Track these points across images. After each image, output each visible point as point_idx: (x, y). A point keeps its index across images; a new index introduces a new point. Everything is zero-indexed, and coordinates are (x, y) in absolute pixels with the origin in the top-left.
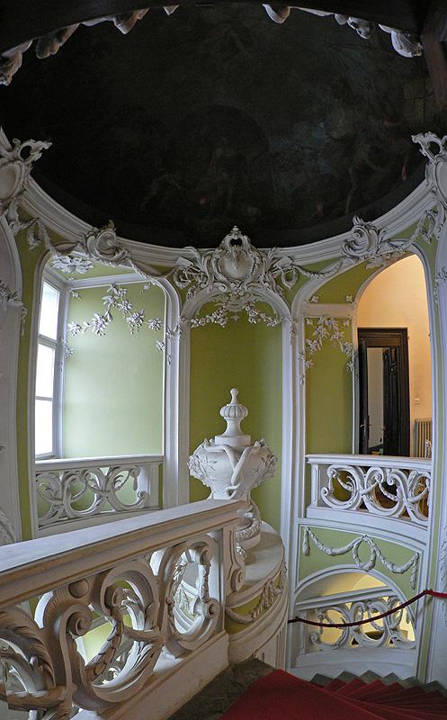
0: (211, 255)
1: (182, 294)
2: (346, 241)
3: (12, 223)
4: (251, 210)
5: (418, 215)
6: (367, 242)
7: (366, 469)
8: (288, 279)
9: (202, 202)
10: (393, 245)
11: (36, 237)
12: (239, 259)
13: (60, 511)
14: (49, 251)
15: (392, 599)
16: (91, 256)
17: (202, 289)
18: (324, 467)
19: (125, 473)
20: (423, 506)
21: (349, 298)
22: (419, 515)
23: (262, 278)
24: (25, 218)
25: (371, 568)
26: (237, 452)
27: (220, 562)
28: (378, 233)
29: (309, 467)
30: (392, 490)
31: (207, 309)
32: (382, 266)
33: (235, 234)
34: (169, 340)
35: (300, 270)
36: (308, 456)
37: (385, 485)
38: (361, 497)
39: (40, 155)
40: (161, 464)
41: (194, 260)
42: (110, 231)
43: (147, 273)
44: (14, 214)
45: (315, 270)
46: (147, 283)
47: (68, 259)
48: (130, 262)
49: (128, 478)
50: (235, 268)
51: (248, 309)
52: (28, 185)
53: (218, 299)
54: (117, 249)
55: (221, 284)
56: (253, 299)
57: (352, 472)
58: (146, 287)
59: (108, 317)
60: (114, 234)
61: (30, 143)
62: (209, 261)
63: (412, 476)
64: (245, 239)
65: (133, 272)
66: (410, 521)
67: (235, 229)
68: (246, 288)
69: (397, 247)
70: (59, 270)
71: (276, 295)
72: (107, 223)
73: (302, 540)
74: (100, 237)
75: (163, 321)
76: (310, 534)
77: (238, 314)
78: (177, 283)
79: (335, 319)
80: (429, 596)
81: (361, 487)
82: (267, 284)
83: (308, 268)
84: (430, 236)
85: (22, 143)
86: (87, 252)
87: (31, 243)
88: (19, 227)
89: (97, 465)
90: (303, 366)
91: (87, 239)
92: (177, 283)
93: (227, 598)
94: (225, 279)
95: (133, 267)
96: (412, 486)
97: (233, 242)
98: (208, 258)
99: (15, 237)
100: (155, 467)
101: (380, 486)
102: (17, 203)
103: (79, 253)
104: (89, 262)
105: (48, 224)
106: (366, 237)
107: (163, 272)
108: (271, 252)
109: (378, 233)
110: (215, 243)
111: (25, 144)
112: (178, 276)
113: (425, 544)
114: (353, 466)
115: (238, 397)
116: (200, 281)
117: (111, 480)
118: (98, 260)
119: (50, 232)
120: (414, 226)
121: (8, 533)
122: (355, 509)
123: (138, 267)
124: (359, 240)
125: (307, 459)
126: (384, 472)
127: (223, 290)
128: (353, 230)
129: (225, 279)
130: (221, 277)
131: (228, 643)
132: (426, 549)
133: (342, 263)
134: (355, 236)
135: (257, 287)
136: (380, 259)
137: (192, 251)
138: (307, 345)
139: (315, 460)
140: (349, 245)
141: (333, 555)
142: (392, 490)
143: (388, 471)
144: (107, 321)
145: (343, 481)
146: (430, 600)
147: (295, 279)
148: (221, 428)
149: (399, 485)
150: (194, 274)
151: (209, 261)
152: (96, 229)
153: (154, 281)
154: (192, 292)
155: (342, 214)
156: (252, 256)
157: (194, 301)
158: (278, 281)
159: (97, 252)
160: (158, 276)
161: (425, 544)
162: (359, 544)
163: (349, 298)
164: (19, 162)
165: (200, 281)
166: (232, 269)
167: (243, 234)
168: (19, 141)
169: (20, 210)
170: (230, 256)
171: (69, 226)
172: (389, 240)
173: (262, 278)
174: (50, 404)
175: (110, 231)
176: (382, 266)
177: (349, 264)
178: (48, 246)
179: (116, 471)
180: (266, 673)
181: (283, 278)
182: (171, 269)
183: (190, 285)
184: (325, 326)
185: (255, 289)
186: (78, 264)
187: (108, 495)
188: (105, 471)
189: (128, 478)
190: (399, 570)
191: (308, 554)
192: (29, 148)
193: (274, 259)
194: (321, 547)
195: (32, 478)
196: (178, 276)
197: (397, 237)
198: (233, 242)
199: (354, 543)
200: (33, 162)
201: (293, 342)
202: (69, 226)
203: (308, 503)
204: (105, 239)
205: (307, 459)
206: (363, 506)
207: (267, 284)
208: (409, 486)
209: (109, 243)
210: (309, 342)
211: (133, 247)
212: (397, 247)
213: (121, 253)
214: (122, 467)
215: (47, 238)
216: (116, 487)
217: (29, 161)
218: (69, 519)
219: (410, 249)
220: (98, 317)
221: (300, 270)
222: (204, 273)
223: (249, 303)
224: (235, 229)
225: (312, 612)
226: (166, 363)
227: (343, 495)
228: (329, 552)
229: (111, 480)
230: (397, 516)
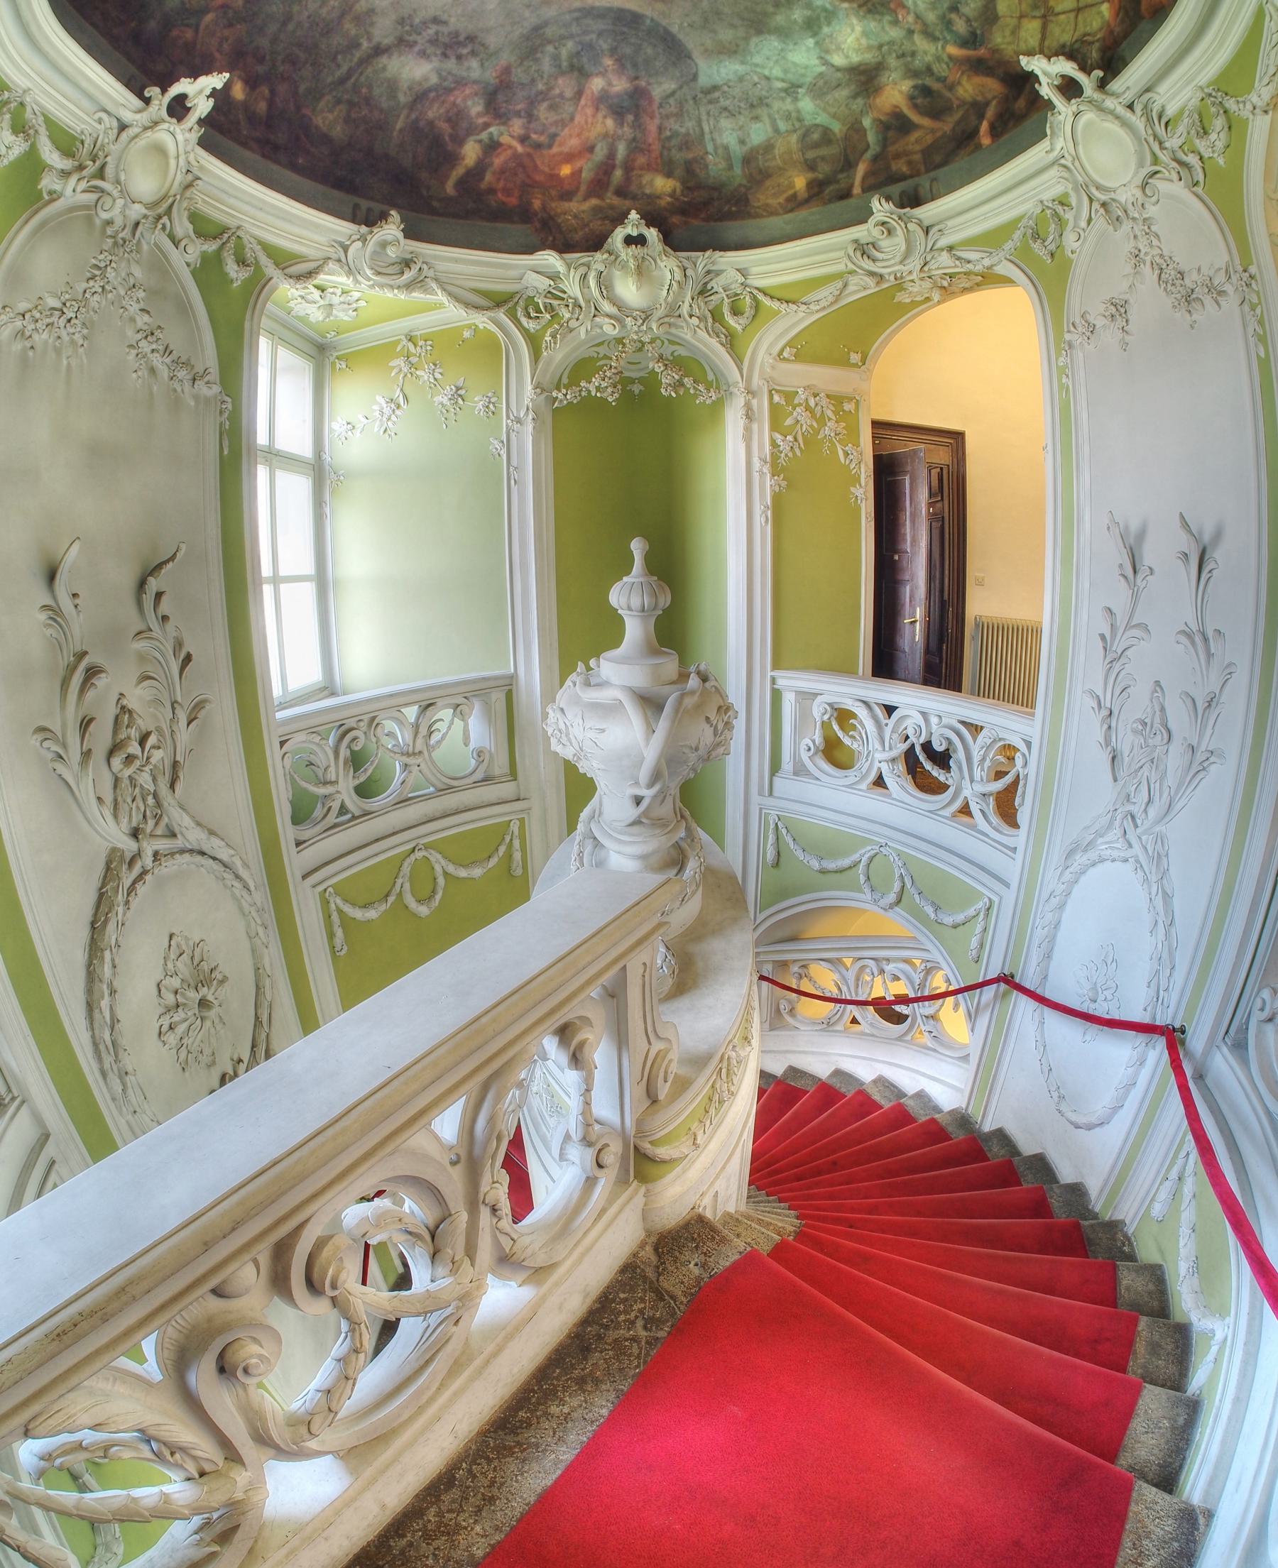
0: (588, 266)
1: (534, 342)
2: (856, 241)
3: (183, 244)
4: (662, 185)
5: (1021, 204)
6: (904, 247)
7: (890, 710)
8: (736, 312)
9: (566, 170)
10: (959, 258)
11: (242, 262)
12: (641, 272)
13: (336, 805)
14: (271, 278)
15: (929, 965)
16: (356, 281)
17: (571, 331)
18: (806, 697)
19: (446, 714)
20: (1006, 807)
21: (855, 358)
22: (995, 820)
23: (685, 310)
24: (205, 228)
25: (891, 906)
26: (650, 703)
27: (621, 1040)
28: (927, 231)
29: (777, 696)
30: (942, 760)
31: (581, 369)
32: (928, 299)
33: (633, 224)
34: (513, 435)
35: (760, 297)
36: (775, 673)
37: (927, 747)
38: (877, 765)
39: (211, 102)
40: (510, 691)
41: (554, 277)
42: (391, 230)
43: (468, 305)
44: (183, 227)
45: (788, 296)
46: (469, 327)
47: (317, 293)
48: (434, 285)
49: (452, 723)
50: (633, 288)
51: (659, 368)
52: (202, 168)
53: (603, 350)
54: (407, 263)
55: (607, 320)
56: (668, 350)
57: (862, 712)
58: (467, 334)
59: (401, 400)
60: (400, 235)
61: (183, 86)
62: (584, 277)
63: (983, 738)
64: (652, 234)
65: (441, 306)
66: (974, 827)
67: (634, 215)
68: (654, 326)
69: (969, 262)
70: (304, 319)
71: (713, 342)
72: (384, 216)
73: (766, 838)
74: (371, 246)
75: (499, 398)
76: (782, 830)
77: (641, 380)
78: (524, 321)
79: (828, 396)
80: (1003, 986)
81: (878, 746)
82: (695, 321)
83: (768, 291)
84: (1052, 247)
85: (164, 91)
86: (350, 272)
87: (233, 275)
88: (196, 249)
89: (394, 702)
90: (767, 485)
91: (346, 249)
92: (524, 321)
93: (639, 1123)
94: (613, 310)
95: (441, 297)
96: (984, 759)
97: (629, 241)
98: (582, 270)
99: (193, 273)
100: (498, 698)
101: (918, 749)
102: (185, 204)
103: (335, 278)
104: (356, 295)
105: (258, 232)
106: (899, 239)
107: (498, 301)
108: (703, 260)
109: (927, 231)
110: (596, 243)
111: (175, 90)
112: (526, 309)
113: (1007, 885)
114: (864, 702)
115: (648, 559)
116: (567, 315)
117: (423, 731)
118: (372, 287)
119: (270, 250)
120: (1012, 225)
121: (237, 877)
122: (864, 786)
123: (450, 294)
124: (885, 243)
125: (773, 680)
126: (927, 721)
127: (610, 330)
128: (872, 221)
129: (613, 310)
130: (607, 307)
131: (644, 1199)
132: (1010, 897)
133: (845, 286)
134: (876, 232)
135: (677, 326)
136: (927, 284)
137: (550, 259)
138: (774, 444)
139: (792, 682)
140: (864, 249)
141: (823, 872)
142: (942, 760)
143: (934, 720)
144: (398, 407)
145: (842, 728)
146: (1005, 995)
147: (749, 312)
148: (616, 624)
149: (955, 751)
150: (555, 303)
151: (584, 277)
152: (364, 229)
153: (482, 321)
154: (554, 336)
155: (845, 195)
156: (667, 266)
157: (558, 355)
158: (716, 316)
159: (369, 272)
160: (487, 309)
161: (1007, 885)
162: (871, 859)
163: (855, 358)
164: (165, 126)
165: (567, 315)
166: (629, 290)
167: (648, 225)
168: (157, 90)
169: (195, 217)
170: (624, 267)
171: (305, 233)
172: (950, 248)
173: (685, 310)
174: (309, 589)
175: (391, 230)
176: (928, 299)
177: (859, 288)
178: (269, 268)
179: (428, 713)
180: (726, 1258)
181: (726, 310)
182: (511, 296)
183: (549, 324)
184: (808, 408)
185: (673, 331)
186: (336, 300)
187: (419, 760)
188: (411, 713)
189: (452, 723)
190: (948, 920)
191: (777, 864)
192: (182, 98)
193: (708, 272)
194: (800, 855)
195: (273, 753)
196: (526, 309)
197: (970, 243)
198: (629, 241)
199: (864, 854)
200: (201, 122)
201: (748, 438)
202: (305, 233)
203: (775, 767)
204: (384, 245)
205: (773, 680)
206: (880, 782)
207: (695, 321)
208: (976, 758)
209: (392, 252)
210: (778, 437)
211: (435, 257)
212: (969, 262)
213: (415, 268)
214: (440, 703)
215: (264, 260)
216: (432, 742)
217: (192, 119)
218: (354, 818)
219: (999, 270)
220: (382, 401)
221: (760, 297)
222: (576, 299)
223: (661, 357)
224: (634, 215)
225: (784, 965)
226: (508, 469)
227: (834, 753)
228: (815, 864)
229: (423, 731)
230: (948, 812)
